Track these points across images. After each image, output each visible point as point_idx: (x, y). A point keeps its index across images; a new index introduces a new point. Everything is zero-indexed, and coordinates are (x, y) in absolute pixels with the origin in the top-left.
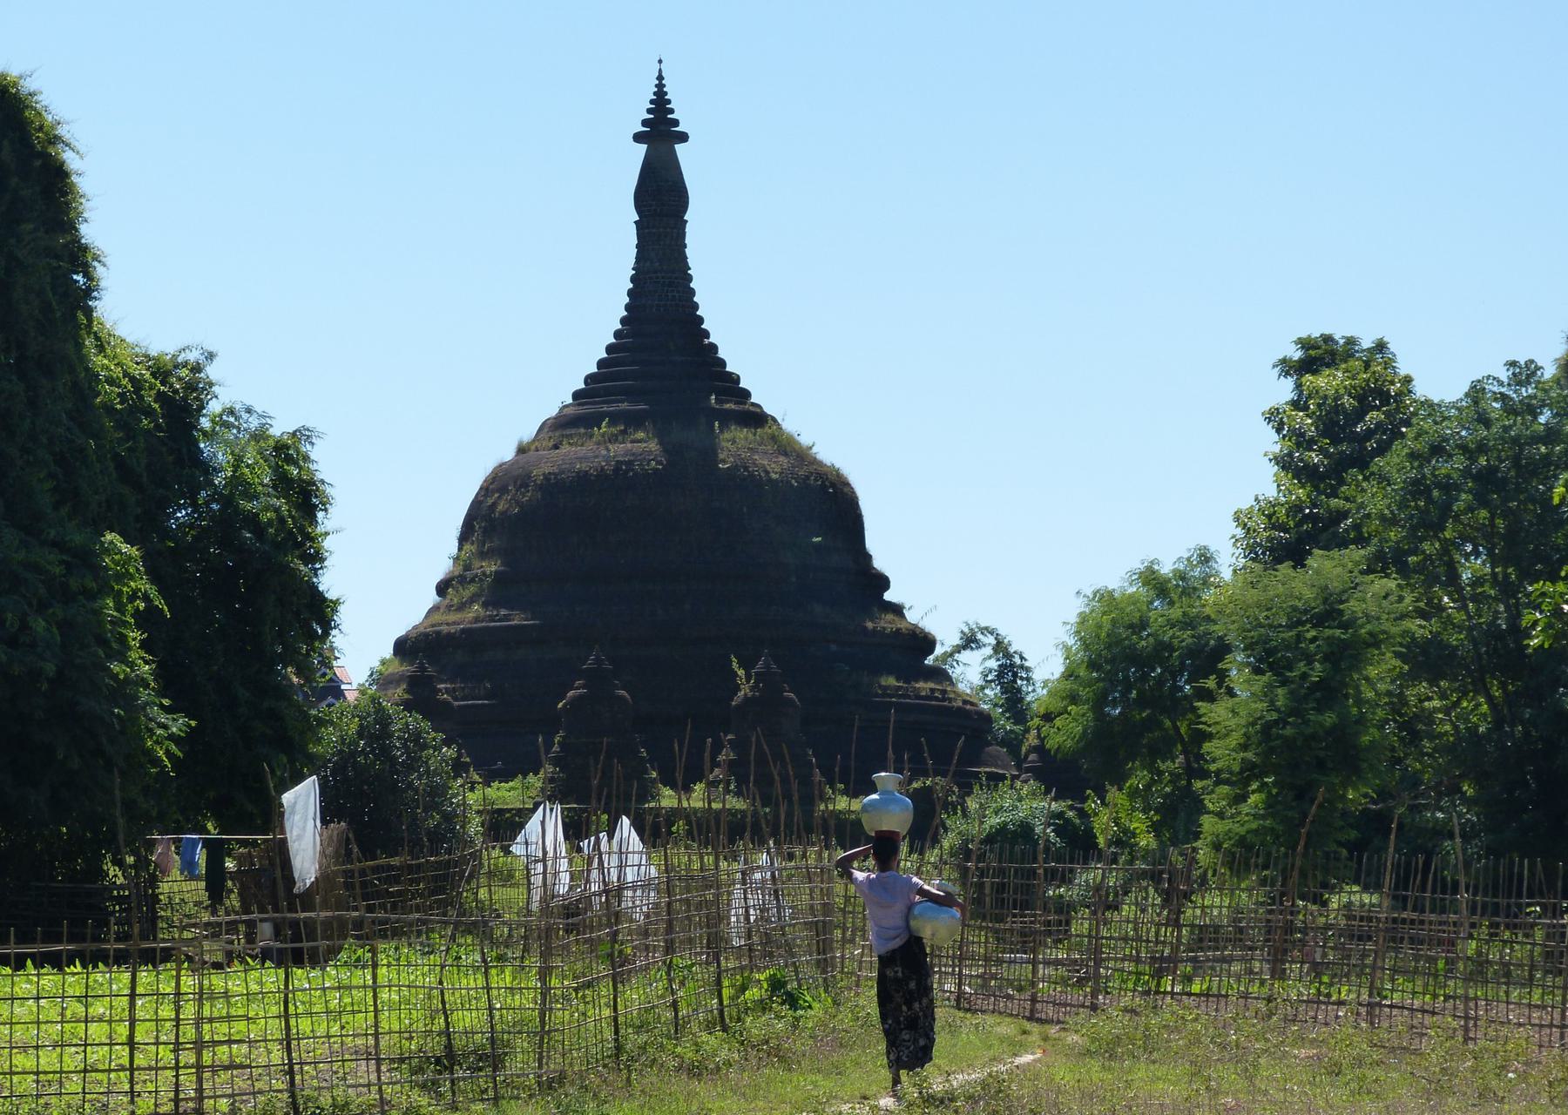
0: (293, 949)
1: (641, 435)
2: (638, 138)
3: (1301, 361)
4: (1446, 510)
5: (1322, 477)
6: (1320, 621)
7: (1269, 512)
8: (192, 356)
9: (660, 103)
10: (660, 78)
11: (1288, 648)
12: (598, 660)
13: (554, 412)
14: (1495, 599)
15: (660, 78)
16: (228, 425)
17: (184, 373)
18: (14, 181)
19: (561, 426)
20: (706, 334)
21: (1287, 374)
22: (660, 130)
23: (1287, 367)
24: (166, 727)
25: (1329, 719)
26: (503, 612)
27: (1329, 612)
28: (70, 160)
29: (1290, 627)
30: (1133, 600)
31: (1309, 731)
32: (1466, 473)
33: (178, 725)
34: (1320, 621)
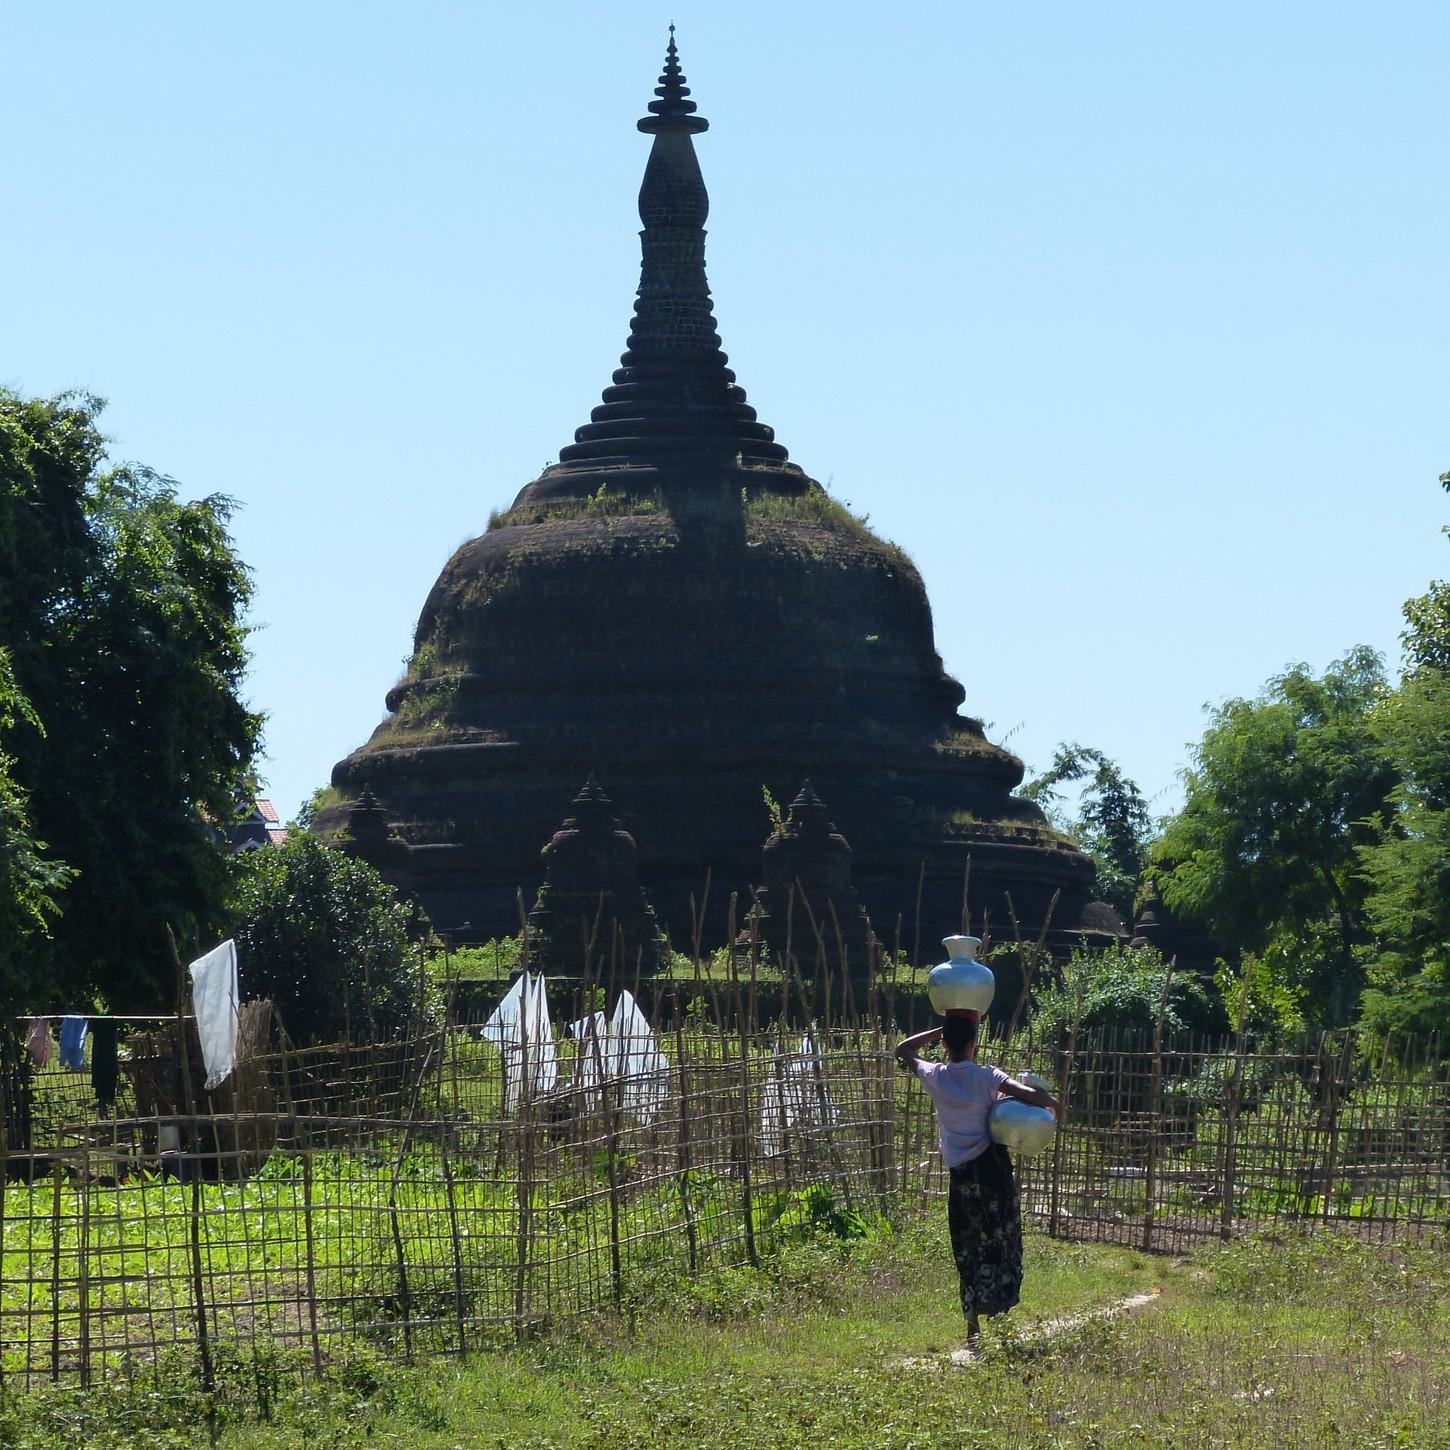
1: (647, 505)
2: (644, 126)
8: (75, 404)
9: (672, 82)
10: (672, 49)
12: (592, 793)
13: (536, 474)
15: (672, 49)
16: (120, 493)
19: (546, 493)
20: (731, 376)
22: (672, 116)
26: (472, 731)
30: (1275, 715)
33: (57, 874)
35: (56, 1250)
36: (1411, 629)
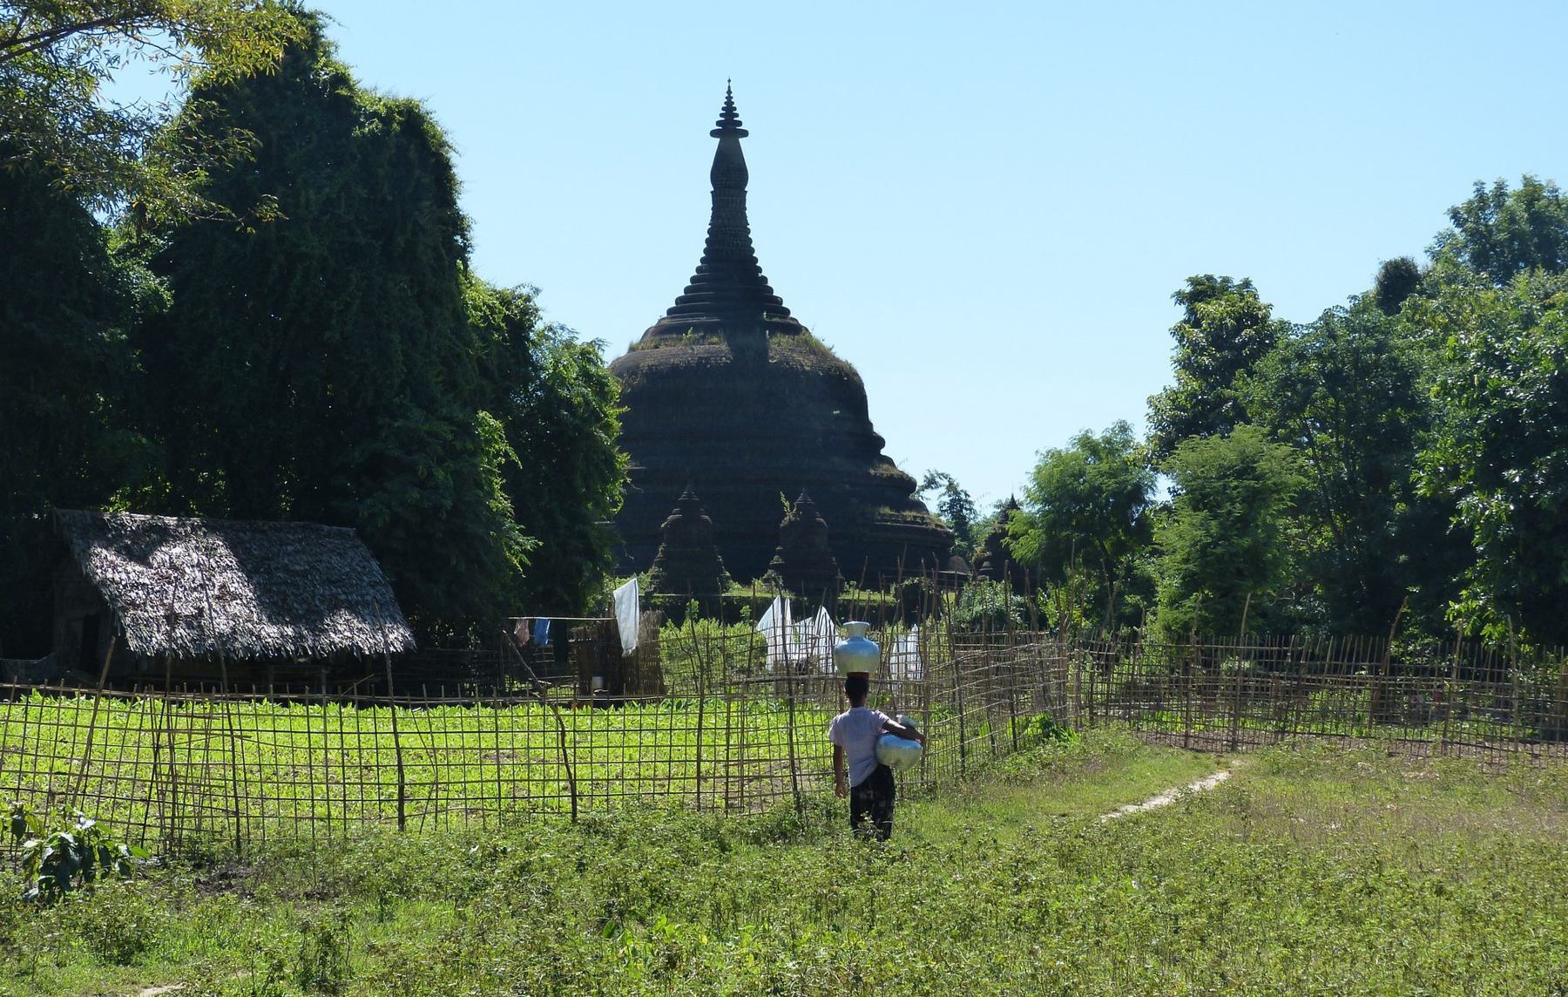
0: (385, 682)
1: (715, 339)
2: (714, 134)
3: (1191, 293)
4: (1307, 399)
5: (1210, 374)
6: (1240, 475)
7: (1173, 397)
8: (525, 291)
9: (729, 110)
10: (729, 92)
11: (1218, 493)
12: (689, 495)
13: (654, 323)
14: (1339, 460)
15: (729, 92)
16: (548, 338)
17: (519, 302)
18: (418, 172)
19: (662, 332)
20: (760, 270)
21: (1181, 302)
22: (729, 128)
23: (1181, 297)
24: (520, 545)
25: (1246, 542)
27: (1246, 469)
28: (454, 158)
29: (1219, 478)
30: (1075, 457)
31: (1233, 550)
32: (1321, 372)
33: (529, 543)
34: (1240, 475)
35: (728, 745)
36: (1151, 411)
